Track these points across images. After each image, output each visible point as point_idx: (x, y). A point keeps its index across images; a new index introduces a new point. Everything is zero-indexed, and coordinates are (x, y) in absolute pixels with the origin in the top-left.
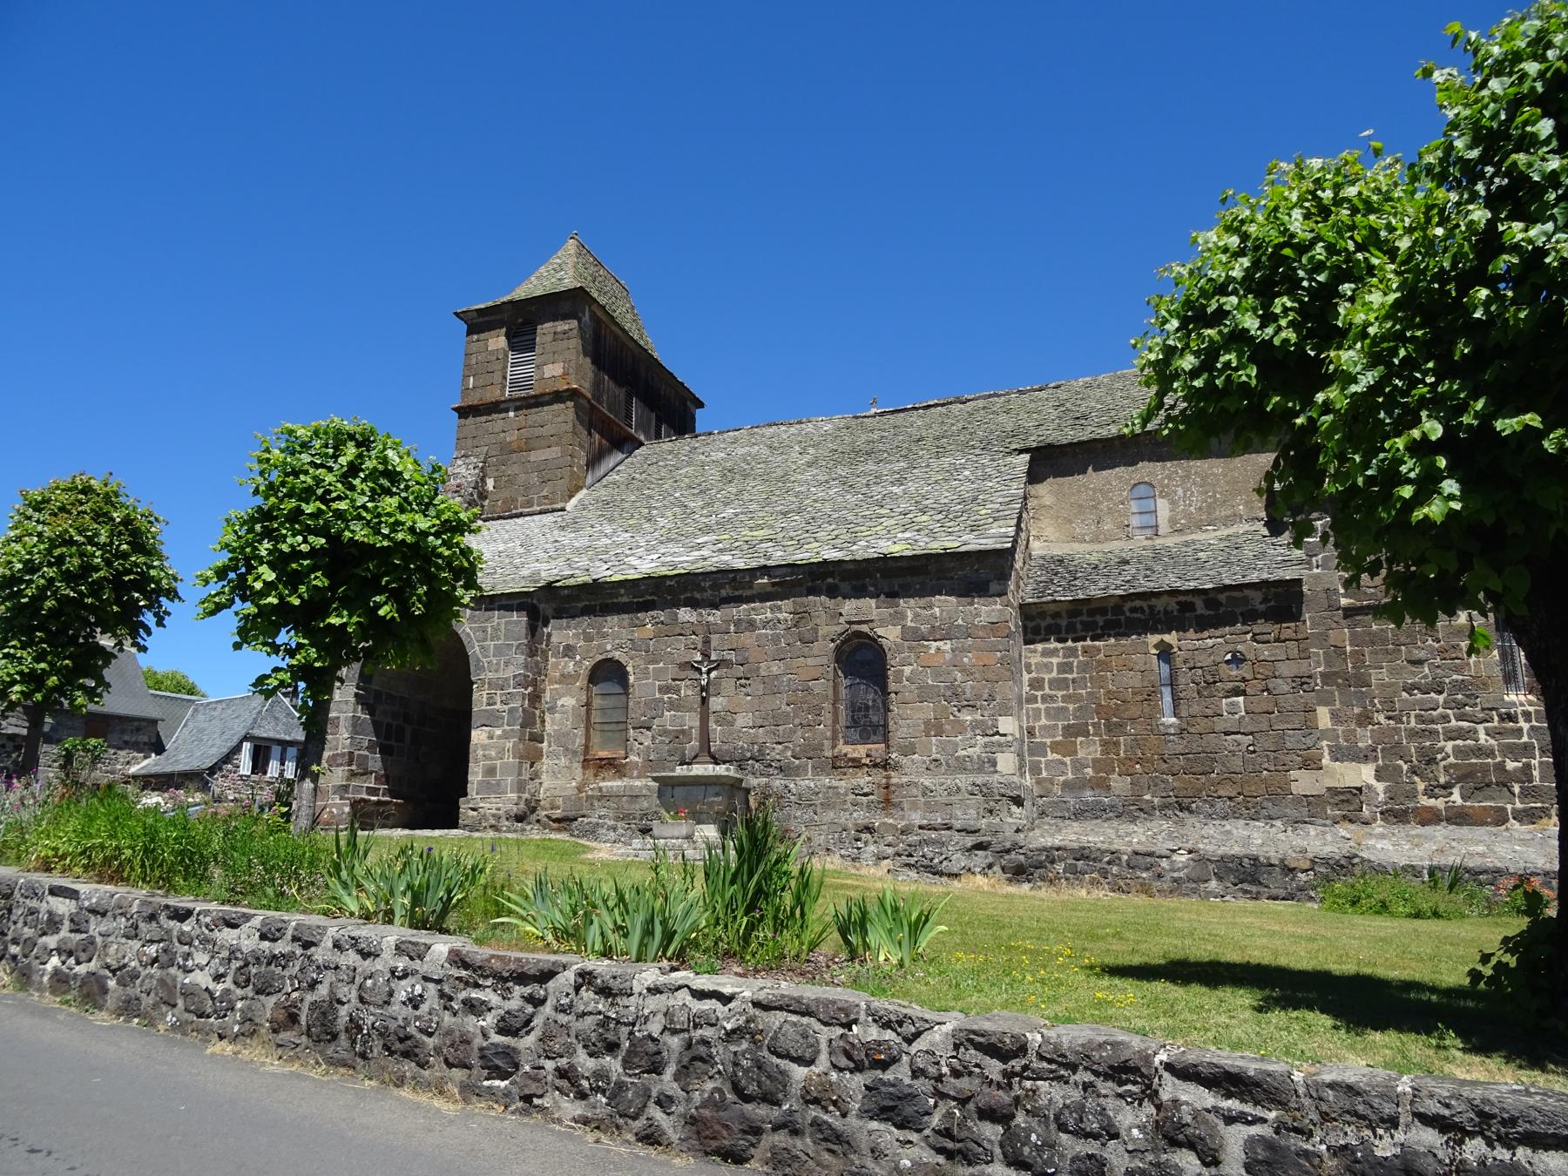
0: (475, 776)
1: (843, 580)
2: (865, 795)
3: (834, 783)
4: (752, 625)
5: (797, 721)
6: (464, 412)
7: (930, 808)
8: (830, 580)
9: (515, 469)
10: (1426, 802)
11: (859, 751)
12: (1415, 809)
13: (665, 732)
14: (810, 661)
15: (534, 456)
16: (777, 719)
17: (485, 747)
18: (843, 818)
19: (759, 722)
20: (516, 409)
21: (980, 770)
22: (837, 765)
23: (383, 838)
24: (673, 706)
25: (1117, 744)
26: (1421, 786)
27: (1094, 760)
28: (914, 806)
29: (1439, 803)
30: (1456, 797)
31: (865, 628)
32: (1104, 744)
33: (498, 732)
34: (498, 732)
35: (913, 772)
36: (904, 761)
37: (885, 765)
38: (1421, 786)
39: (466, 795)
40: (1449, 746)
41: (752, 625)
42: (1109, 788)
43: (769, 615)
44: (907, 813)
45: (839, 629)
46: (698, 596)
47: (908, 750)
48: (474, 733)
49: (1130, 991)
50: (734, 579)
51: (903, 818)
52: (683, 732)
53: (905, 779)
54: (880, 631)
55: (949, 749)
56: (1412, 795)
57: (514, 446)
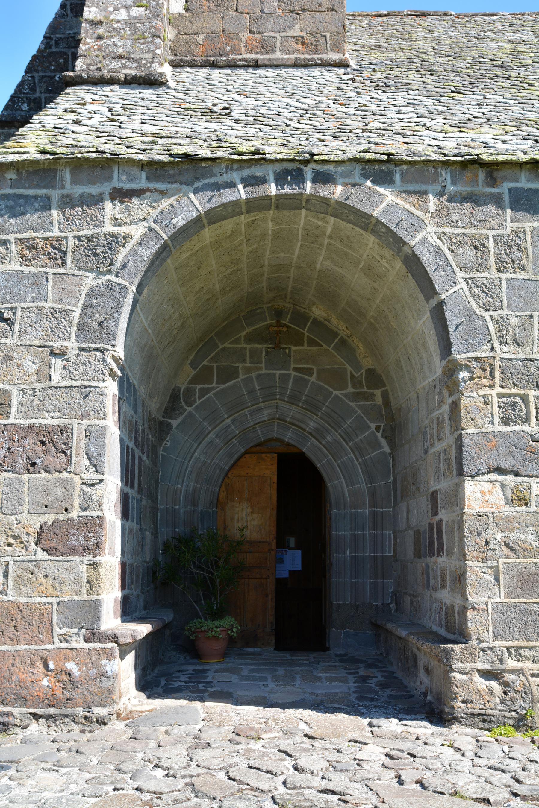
17: (503, 523)
39: (462, 636)
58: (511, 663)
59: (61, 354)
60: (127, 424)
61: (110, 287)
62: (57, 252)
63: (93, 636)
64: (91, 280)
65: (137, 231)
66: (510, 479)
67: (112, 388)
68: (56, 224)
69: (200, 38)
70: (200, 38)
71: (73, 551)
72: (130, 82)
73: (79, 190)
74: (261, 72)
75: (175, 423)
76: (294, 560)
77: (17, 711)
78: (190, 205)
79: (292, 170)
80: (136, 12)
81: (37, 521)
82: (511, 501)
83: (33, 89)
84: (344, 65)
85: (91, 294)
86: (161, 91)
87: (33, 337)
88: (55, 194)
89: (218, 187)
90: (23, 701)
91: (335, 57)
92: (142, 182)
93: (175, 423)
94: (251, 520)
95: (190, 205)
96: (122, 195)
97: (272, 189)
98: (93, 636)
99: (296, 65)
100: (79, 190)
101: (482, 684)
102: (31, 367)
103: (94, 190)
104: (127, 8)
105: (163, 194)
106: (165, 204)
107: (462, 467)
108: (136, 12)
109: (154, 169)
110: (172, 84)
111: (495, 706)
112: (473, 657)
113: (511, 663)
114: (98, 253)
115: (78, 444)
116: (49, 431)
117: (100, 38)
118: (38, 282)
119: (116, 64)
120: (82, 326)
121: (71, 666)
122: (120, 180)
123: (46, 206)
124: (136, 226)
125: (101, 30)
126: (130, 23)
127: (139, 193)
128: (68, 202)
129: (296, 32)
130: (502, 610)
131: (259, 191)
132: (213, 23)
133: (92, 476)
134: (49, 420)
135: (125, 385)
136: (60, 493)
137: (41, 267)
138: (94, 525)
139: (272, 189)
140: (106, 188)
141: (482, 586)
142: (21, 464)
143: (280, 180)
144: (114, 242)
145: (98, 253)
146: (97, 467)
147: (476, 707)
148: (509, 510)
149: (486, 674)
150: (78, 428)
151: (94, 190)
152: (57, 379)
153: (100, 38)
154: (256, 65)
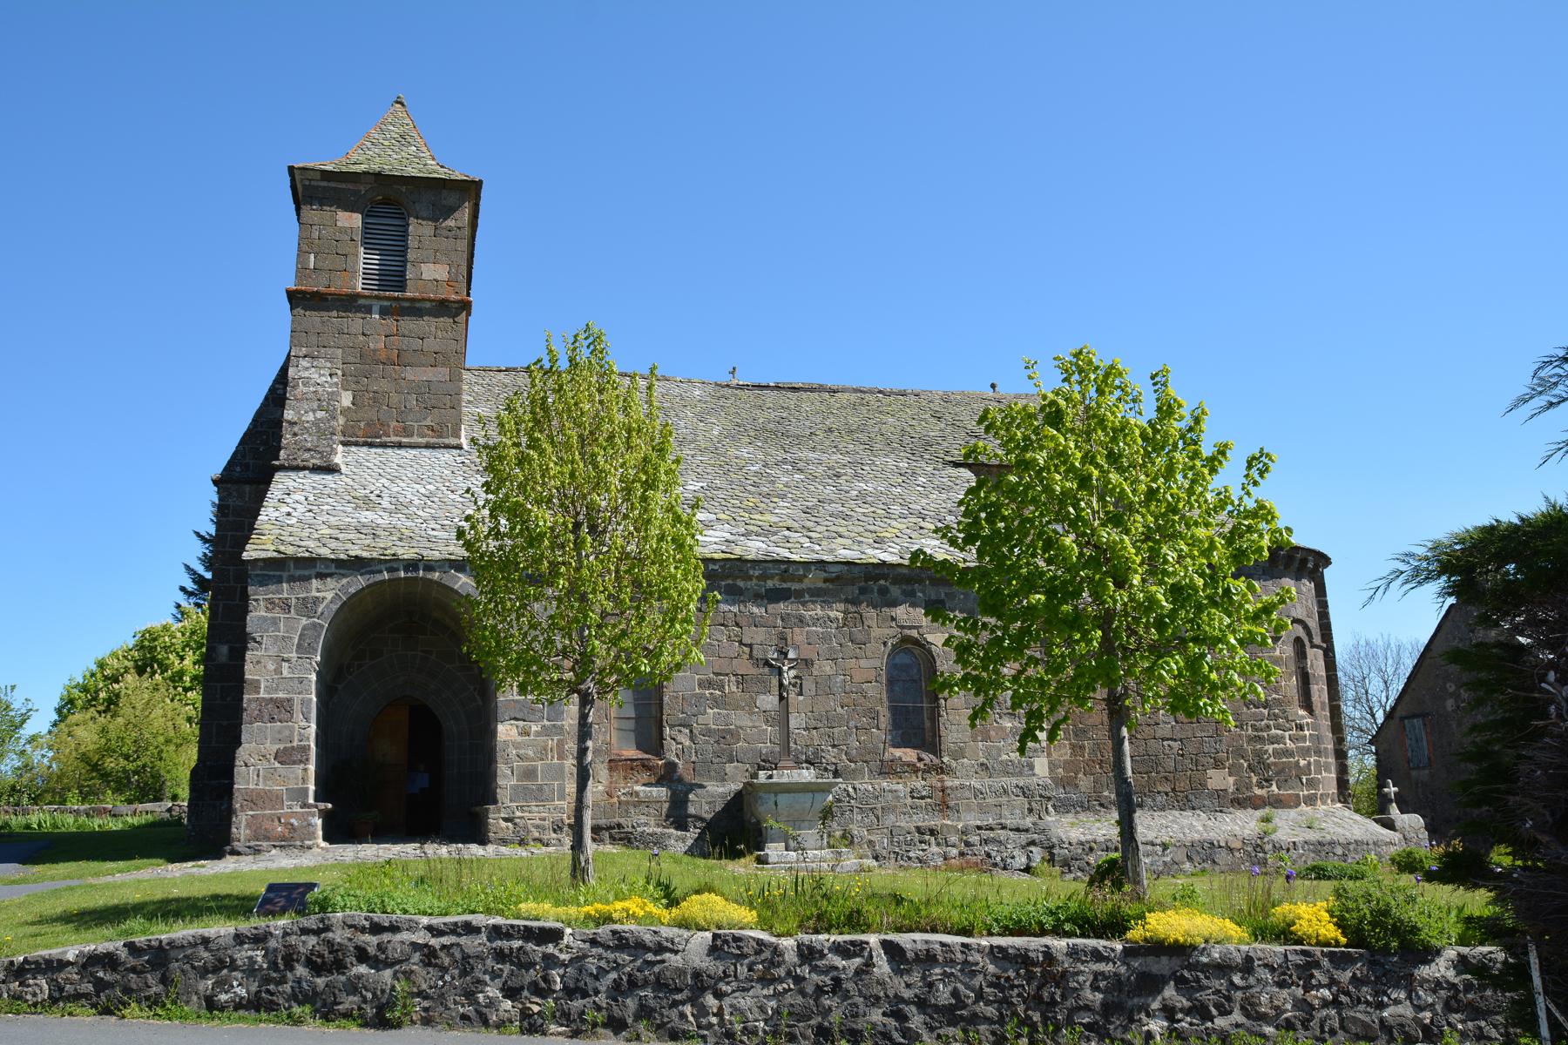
0: (506, 780)
1: (893, 583)
2: (923, 798)
3: (895, 787)
4: (801, 621)
5: (852, 724)
6: (295, 298)
7: (983, 810)
8: (882, 582)
9: (384, 385)
10: (1258, 792)
11: (909, 755)
12: (1250, 798)
13: (708, 732)
14: (863, 663)
15: (410, 374)
16: (830, 721)
17: (517, 745)
18: (903, 823)
19: (813, 723)
20: (384, 312)
21: (1021, 774)
22: (888, 769)
23: (481, 861)
24: (717, 703)
25: (1082, 748)
26: (1255, 780)
27: (1066, 762)
28: (969, 809)
29: (1258, 792)
30: (1274, 787)
31: (914, 633)
32: (1073, 747)
33: (535, 728)
34: (535, 728)
35: (964, 777)
36: (954, 764)
37: (941, 770)
38: (1255, 780)
39: (495, 802)
40: (1270, 748)
41: (801, 621)
42: (1077, 786)
43: (819, 612)
44: (963, 815)
45: (891, 632)
46: (741, 583)
47: (958, 754)
48: (501, 728)
49: (45, 928)
50: (786, 571)
51: (959, 819)
52: (729, 731)
53: (957, 782)
54: (930, 638)
55: (994, 752)
56: (1249, 787)
57: (383, 357)
58: (518, 814)
59: (288, 661)
60: (318, 696)
61: (314, 625)
62: (286, 607)
63: (305, 805)
64: (304, 621)
65: (329, 596)
66: (521, 723)
67: (314, 677)
68: (285, 591)
69: (362, 425)
70: (362, 425)
71: (294, 763)
72: (316, 469)
73: (298, 573)
74: (402, 452)
75: (340, 687)
76: (422, 781)
77: (265, 844)
78: (360, 581)
79: (412, 565)
80: (320, 414)
81: (275, 747)
82: (520, 734)
83: (244, 457)
84: (459, 447)
85: (304, 628)
86: (336, 476)
87: (273, 651)
88: (285, 575)
89: (373, 572)
90: (268, 839)
91: (453, 441)
92: (333, 570)
93: (340, 687)
94: (389, 750)
95: (360, 581)
96: (321, 576)
97: (402, 574)
98: (305, 805)
99: (427, 446)
100: (298, 573)
101: (503, 824)
102: (271, 667)
103: (306, 573)
104: (314, 411)
105: (344, 576)
106: (344, 581)
107: (930, 652)
108: (320, 414)
109: (339, 563)
110: (343, 469)
111: (509, 835)
112: (499, 811)
113: (518, 814)
114: (309, 606)
115: (297, 707)
116: (282, 701)
117: (295, 435)
118: (275, 621)
119: (307, 455)
120: (299, 646)
121: (293, 821)
122: (321, 568)
123: (280, 581)
124: (328, 593)
125: (296, 429)
126: (316, 423)
127: (331, 575)
128: (292, 579)
129: (428, 422)
130: (514, 788)
131: (395, 575)
132: (372, 414)
133: (304, 724)
134: (281, 695)
135: (319, 674)
136: (287, 733)
137: (277, 613)
138: (306, 749)
139: (402, 574)
140: (313, 572)
141: (505, 776)
142: (266, 718)
143: (406, 570)
144: (316, 601)
145: (309, 606)
146: (307, 720)
147: (500, 835)
148: (520, 739)
149: (506, 820)
150: (297, 698)
151: (306, 573)
152: (285, 673)
153: (295, 435)
154: (400, 446)
